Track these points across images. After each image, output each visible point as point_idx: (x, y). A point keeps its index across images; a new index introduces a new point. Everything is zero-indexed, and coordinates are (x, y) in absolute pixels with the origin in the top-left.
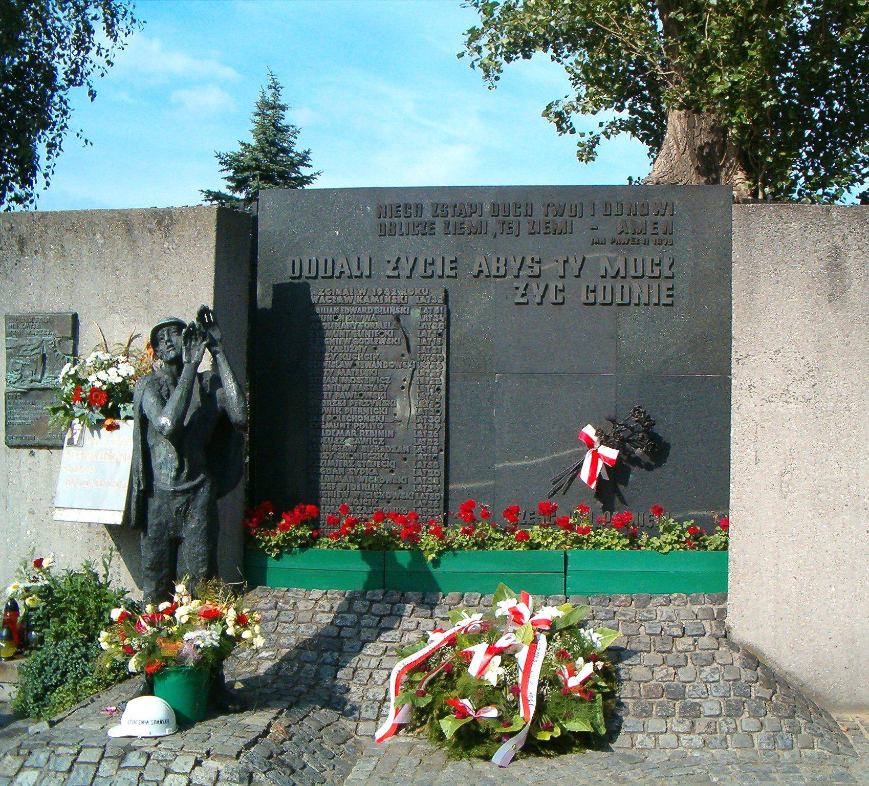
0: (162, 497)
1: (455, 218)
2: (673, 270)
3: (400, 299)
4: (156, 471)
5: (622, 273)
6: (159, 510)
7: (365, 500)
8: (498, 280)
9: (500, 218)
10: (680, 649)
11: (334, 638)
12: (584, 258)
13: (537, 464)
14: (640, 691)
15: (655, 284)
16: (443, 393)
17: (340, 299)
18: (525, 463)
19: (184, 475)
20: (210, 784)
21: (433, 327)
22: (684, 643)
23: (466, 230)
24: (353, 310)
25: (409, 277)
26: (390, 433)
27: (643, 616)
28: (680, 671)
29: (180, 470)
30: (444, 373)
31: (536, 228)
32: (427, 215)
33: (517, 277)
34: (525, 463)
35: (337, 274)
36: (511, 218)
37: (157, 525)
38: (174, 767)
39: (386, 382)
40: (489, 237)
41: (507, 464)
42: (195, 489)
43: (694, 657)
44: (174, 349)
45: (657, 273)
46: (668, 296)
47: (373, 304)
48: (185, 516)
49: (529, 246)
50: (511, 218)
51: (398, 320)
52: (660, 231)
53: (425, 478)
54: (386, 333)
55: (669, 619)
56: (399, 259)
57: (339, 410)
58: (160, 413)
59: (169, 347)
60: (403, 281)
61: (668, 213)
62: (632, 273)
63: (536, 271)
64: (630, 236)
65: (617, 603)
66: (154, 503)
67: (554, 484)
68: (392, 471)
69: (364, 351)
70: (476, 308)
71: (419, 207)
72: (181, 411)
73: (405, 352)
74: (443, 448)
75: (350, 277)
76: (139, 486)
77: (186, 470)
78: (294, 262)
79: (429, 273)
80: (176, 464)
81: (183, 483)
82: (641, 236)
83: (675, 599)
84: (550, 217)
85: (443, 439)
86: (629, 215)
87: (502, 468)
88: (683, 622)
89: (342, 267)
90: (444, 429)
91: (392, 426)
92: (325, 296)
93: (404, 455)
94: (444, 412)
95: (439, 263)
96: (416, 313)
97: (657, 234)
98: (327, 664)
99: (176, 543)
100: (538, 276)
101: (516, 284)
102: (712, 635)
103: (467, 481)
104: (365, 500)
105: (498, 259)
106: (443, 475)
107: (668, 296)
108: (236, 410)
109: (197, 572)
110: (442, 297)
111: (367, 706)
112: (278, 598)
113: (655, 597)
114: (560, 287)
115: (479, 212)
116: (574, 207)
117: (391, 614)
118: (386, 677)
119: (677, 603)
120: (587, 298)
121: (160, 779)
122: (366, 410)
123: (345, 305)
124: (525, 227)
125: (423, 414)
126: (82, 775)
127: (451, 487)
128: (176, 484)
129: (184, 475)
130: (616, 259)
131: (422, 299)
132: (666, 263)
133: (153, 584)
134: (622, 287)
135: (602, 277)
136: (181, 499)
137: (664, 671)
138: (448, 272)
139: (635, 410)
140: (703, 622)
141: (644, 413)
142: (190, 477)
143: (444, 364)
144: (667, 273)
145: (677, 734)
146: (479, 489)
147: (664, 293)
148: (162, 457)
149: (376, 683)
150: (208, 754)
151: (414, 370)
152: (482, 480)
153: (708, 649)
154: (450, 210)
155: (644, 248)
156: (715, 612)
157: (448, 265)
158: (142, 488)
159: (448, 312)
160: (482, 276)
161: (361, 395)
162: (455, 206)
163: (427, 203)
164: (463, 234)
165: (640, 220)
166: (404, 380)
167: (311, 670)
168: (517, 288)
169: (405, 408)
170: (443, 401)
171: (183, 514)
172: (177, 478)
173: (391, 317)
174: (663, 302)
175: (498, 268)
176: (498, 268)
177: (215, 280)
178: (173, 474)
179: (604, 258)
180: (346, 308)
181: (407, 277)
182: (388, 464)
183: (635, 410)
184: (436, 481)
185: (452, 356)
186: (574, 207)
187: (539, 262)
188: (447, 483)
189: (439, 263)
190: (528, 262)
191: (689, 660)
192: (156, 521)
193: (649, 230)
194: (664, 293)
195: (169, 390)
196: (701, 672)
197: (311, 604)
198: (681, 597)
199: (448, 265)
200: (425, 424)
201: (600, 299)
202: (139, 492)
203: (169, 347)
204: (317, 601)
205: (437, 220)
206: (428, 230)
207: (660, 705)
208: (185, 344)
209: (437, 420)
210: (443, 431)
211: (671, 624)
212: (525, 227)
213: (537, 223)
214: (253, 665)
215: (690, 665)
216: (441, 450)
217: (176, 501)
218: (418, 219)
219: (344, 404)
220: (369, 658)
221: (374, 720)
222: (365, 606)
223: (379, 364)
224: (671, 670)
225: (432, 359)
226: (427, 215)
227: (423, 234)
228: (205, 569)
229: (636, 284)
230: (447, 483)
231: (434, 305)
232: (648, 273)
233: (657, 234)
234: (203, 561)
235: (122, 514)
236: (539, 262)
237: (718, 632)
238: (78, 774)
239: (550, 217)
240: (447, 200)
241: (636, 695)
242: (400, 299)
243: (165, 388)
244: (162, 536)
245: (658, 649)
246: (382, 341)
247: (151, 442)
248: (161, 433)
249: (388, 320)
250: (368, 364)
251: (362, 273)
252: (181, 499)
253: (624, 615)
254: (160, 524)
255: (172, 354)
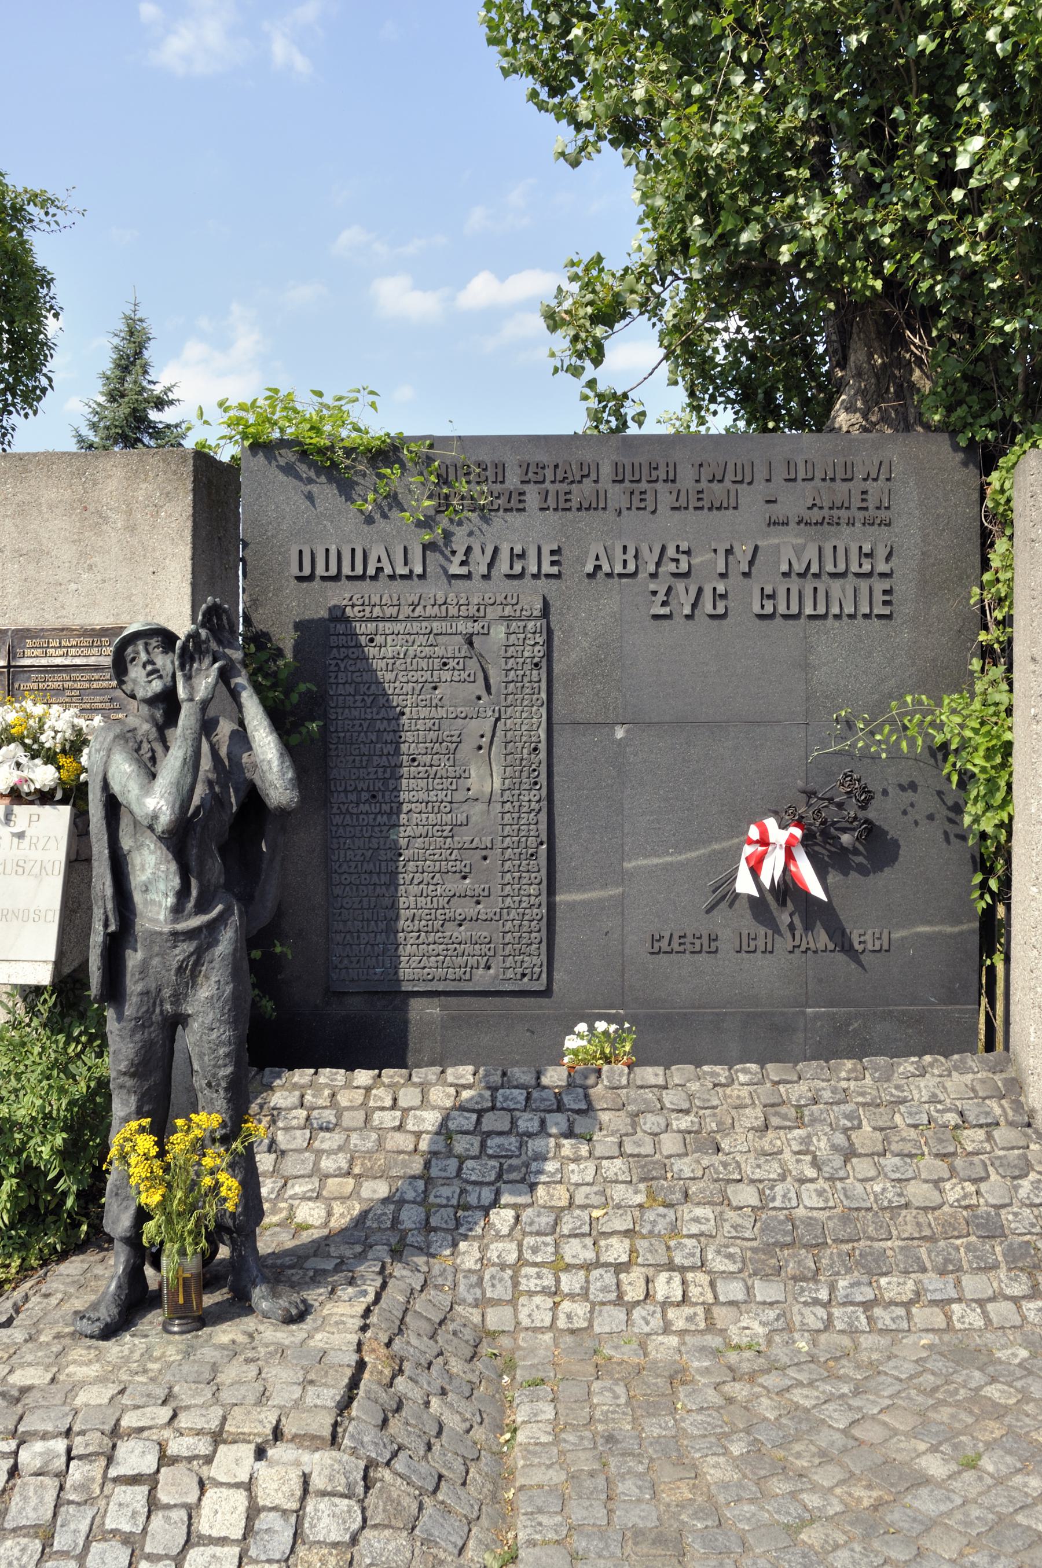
0: (149, 947)
1: (558, 486)
2: (891, 564)
3: (473, 610)
4: (138, 898)
5: (815, 569)
6: (144, 968)
7: (423, 923)
8: (624, 580)
9: (627, 484)
10: (969, 1149)
11: (409, 1153)
12: (756, 548)
13: (688, 860)
14: (930, 1225)
15: (864, 585)
16: (543, 755)
17: (377, 611)
18: (669, 859)
19: (190, 905)
20: (346, 1566)
21: (526, 654)
22: (972, 1139)
23: (574, 504)
24: (399, 627)
25: (486, 577)
26: (461, 818)
27: (892, 1095)
28: (984, 1187)
29: (183, 894)
30: (544, 725)
31: (683, 502)
32: (513, 480)
33: (654, 576)
34: (669, 859)
35: (371, 571)
36: (644, 485)
37: (141, 994)
38: (216, 1472)
39: (454, 739)
40: (609, 515)
41: (642, 862)
42: (212, 928)
43: (997, 1163)
44: (160, 677)
45: (867, 568)
46: (885, 603)
47: (428, 618)
48: (194, 975)
49: (672, 528)
50: (644, 485)
51: (471, 643)
52: (871, 504)
53: (516, 887)
54: (452, 663)
55: (934, 1100)
56: (469, 549)
57: (379, 784)
58: (146, 789)
59: (149, 674)
60: (477, 582)
61: (882, 477)
62: (829, 568)
63: (684, 567)
64: (826, 512)
65: (843, 1074)
66: (134, 959)
67: (714, 892)
68: (465, 878)
69: (417, 692)
70: (589, 620)
71: (500, 468)
72: (186, 788)
73: (483, 693)
74: (545, 839)
75: (392, 577)
76: (106, 925)
77: (194, 893)
78: (301, 552)
79: (518, 569)
80: (176, 882)
81: (189, 916)
82: (843, 513)
83: (931, 1065)
84: (704, 484)
85: (543, 826)
86: (824, 480)
87: (634, 868)
88: (958, 1103)
89: (379, 561)
90: (545, 810)
91: (465, 807)
92: (353, 606)
93: (484, 853)
94: (545, 783)
95: (532, 554)
96: (499, 632)
97: (866, 509)
98: (408, 1202)
99: (177, 1021)
100: (686, 575)
101: (652, 587)
102: (1011, 1124)
103: (581, 888)
104: (423, 923)
105: (625, 547)
106: (545, 882)
107: (885, 603)
108: (278, 783)
109: (214, 1075)
110: (539, 606)
111: (493, 1277)
112: (302, 1087)
113: (899, 1064)
114: (721, 590)
115: (593, 476)
116: (739, 467)
117: (493, 1108)
118: (512, 1221)
119: (936, 1072)
120: (763, 607)
121: (192, 1499)
122: (422, 783)
123: (383, 619)
124: (666, 499)
125: (512, 787)
126: (34, 1501)
127: (558, 898)
128: (175, 921)
129: (190, 905)
130: (804, 547)
131: (508, 611)
132: (881, 553)
133: (133, 1099)
134: (815, 589)
135: (784, 574)
136: (187, 947)
137: (958, 1188)
138: (546, 568)
139: (846, 776)
140: (987, 1102)
141: (859, 781)
142: (201, 907)
143: (543, 711)
144: (882, 567)
145: (1015, 1300)
146: (600, 900)
147: (879, 597)
148: (149, 872)
149: (498, 1232)
150: (277, 1434)
151: (498, 720)
152: (605, 886)
153: (1013, 1148)
154: (549, 473)
155: (846, 530)
156: (1000, 1084)
157: (546, 559)
158: (112, 928)
159: (550, 632)
160: (600, 575)
161: (414, 760)
162: (556, 466)
163: (511, 461)
164: (569, 509)
165: (842, 487)
166: (482, 736)
167: (385, 1214)
168: (654, 593)
169: (485, 778)
170: (543, 768)
171: (189, 973)
172: (177, 910)
173: (460, 639)
174: (876, 611)
175: (625, 561)
176: (625, 561)
177: (193, 573)
178: (170, 901)
179: (790, 549)
180: (388, 625)
181: (484, 577)
182: (459, 866)
183: (846, 776)
184: (534, 891)
185: (557, 698)
186: (739, 467)
187: (688, 553)
188: (551, 891)
189: (532, 554)
190: (671, 552)
191: (990, 1169)
192: (139, 988)
193: (856, 503)
194: (879, 597)
195: (153, 751)
196: (1016, 1188)
197: (358, 1096)
198: (937, 1060)
199: (546, 559)
200: (516, 804)
201: (782, 609)
202: (107, 935)
203: (149, 674)
204: (368, 1089)
205: (526, 488)
206: (515, 503)
207: (968, 1248)
208: (182, 667)
209: (533, 797)
210: (543, 817)
211: (939, 1107)
212: (666, 499)
213: (683, 494)
214: (281, 1210)
215: (994, 1177)
216: (542, 843)
217: (177, 951)
218: (497, 488)
219: (387, 775)
220: (477, 1189)
221: (508, 1302)
222: (448, 1096)
223: (442, 713)
224: (970, 1188)
225: (525, 703)
226: (513, 480)
227: (506, 510)
228: (229, 1070)
229: (836, 585)
230: (551, 891)
231: (530, 618)
232: (854, 568)
233: (866, 509)
234: (226, 1056)
235: (50, 967)
236: (688, 553)
237: (1018, 1118)
238: (25, 1499)
239: (704, 484)
240: (542, 457)
241: (927, 1232)
242: (473, 610)
243: (146, 746)
244: (150, 1012)
245: (934, 1151)
246: (446, 675)
247: (126, 842)
248: (151, 828)
249: (453, 645)
250: (424, 712)
251: (411, 571)
252: (187, 947)
253: (863, 1094)
254: (146, 993)
255: (157, 686)
